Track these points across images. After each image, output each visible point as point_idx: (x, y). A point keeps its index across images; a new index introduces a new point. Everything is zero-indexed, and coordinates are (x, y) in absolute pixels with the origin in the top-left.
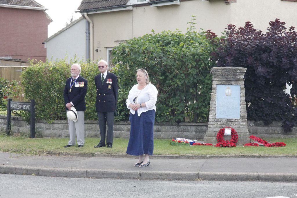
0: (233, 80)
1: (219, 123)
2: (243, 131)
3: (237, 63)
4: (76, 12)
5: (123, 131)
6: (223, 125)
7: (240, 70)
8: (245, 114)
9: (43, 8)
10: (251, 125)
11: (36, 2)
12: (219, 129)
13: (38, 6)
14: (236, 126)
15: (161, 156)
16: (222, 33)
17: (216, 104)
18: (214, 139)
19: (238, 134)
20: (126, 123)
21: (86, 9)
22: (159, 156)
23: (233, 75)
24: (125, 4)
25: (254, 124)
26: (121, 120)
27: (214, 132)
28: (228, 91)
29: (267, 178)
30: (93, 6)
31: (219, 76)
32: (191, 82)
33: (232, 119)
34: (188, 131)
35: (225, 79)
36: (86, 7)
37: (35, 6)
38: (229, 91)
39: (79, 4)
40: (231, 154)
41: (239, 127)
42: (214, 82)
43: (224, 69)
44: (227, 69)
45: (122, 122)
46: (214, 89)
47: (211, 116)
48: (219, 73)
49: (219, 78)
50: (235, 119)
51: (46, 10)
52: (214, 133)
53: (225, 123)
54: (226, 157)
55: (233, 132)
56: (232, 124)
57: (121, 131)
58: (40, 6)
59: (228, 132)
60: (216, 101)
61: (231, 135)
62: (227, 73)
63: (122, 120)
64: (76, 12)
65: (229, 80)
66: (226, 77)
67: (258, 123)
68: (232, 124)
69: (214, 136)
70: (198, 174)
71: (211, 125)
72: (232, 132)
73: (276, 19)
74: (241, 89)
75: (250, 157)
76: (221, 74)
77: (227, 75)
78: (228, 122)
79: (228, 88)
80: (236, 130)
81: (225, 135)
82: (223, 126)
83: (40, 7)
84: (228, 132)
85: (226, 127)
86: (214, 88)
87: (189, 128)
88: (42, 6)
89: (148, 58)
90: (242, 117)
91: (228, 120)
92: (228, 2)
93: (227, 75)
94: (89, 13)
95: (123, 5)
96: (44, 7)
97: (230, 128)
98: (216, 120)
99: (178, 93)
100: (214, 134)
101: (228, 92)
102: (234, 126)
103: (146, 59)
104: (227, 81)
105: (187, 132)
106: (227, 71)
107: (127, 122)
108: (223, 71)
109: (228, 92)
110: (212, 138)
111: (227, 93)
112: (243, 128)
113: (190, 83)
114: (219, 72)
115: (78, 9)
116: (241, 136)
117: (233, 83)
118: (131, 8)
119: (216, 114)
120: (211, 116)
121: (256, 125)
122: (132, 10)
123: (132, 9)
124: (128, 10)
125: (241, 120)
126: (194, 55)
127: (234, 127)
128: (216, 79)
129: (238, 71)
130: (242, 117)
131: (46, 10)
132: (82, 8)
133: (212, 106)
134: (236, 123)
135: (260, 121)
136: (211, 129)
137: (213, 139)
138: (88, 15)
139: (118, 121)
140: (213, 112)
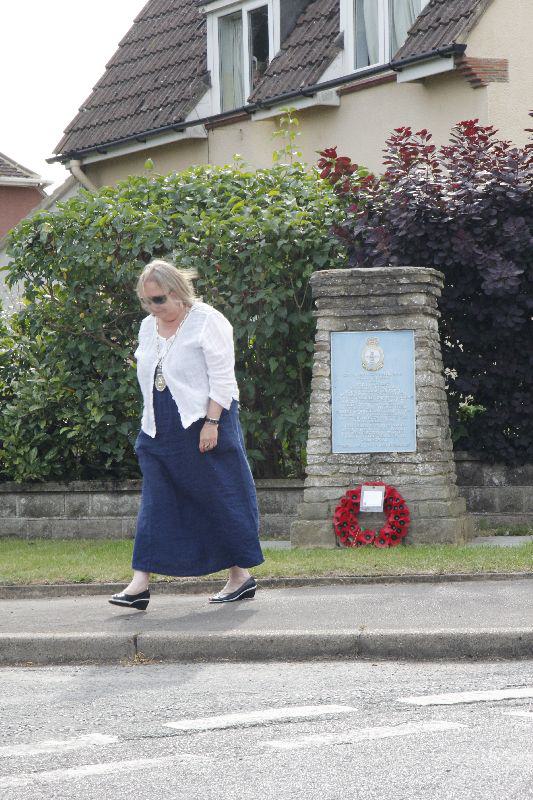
0: (388, 314)
1: (344, 469)
2: (427, 493)
3: (412, 251)
4: (50, 161)
5: (58, 515)
6: (358, 474)
7: (408, 275)
8: (440, 434)
9: (37, 181)
10: (496, 481)
11: (14, 163)
12: (342, 492)
13: (19, 175)
14: (404, 478)
15: (88, 588)
16: (385, 163)
17: (330, 402)
18: (326, 527)
19: (410, 506)
20: (66, 489)
21: (78, 149)
22: (80, 588)
23: (384, 295)
24: (182, 120)
25: (506, 476)
26: (48, 479)
27: (328, 500)
28: (372, 353)
29: (392, 645)
30: (95, 137)
31: (338, 302)
32: (269, 333)
33: (388, 454)
34: (280, 511)
35: (357, 312)
36: (78, 143)
37: (10, 176)
38: (376, 353)
39: (58, 136)
40: (338, 574)
41: (413, 483)
42: (321, 324)
43: (351, 275)
44: (361, 275)
45: (51, 486)
46: (321, 348)
47: (313, 447)
48: (335, 289)
49: (336, 307)
50: (400, 454)
51: (45, 185)
52: (326, 504)
53: (363, 469)
54: (316, 583)
55: (392, 500)
56: (389, 472)
57: (48, 515)
58: (28, 173)
59: (372, 499)
60: (330, 391)
61: (381, 510)
62: (362, 287)
63: (53, 477)
64: (50, 161)
65: (371, 312)
66: (362, 302)
67: (520, 472)
68: (389, 472)
69: (324, 515)
70: (135, 639)
71: (316, 479)
72: (386, 501)
73: (504, 64)
74: (420, 344)
75: (403, 580)
76: (343, 293)
77: (366, 296)
78: (374, 465)
79: (371, 342)
80: (406, 494)
81: (361, 510)
82: (354, 478)
83: (27, 177)
84: (372, 499)
85: (367, 484)
86: (320, 343)
87: (279, 497)
88: (31, 173)
89: (116, 254)
90: (425, 446)
91: (376, 459)
92: (479, 80)
93: (366, 296)
94: (87, 162)
95: (176, 122)
96: (39, 177)
97: (381, 484)
98: (331, 459)
99: (516, 445)
100: (323, 509)
101: (372, 357)
102: (397, 480)
103: (109, 259)
104: (367, 317)
105: (275, 512)
106: (363, 282)
107: (67, 485)
108: (350, 281)
109: (372, 357)
110: (316, 522)
111: (368, 361)
112: (430, 485)
113: (264, 335)
114: (333, 285)
115: (57, 151)
116: (423, 512)
117: (388, 322)
118: (198, 131)
119: (330, 438)
120: (314, 446)
121: (512, 482)
122: (206, 139)
123: (205, 136)
124: (190, 139)
125: (419, 457)
126: (272, 238)
127: (397, 483)
128: (327, 312)
129: (404, 280)
130: (424, 443)
131: (45, 185)
132: (66, 149)
133: (317, 409)
134: (404, 468)
135: (522, 465)
136: (315, 492)
137: (321, 526)
138: (84, 169)
139: (37, 481)
140: (320, 430)
